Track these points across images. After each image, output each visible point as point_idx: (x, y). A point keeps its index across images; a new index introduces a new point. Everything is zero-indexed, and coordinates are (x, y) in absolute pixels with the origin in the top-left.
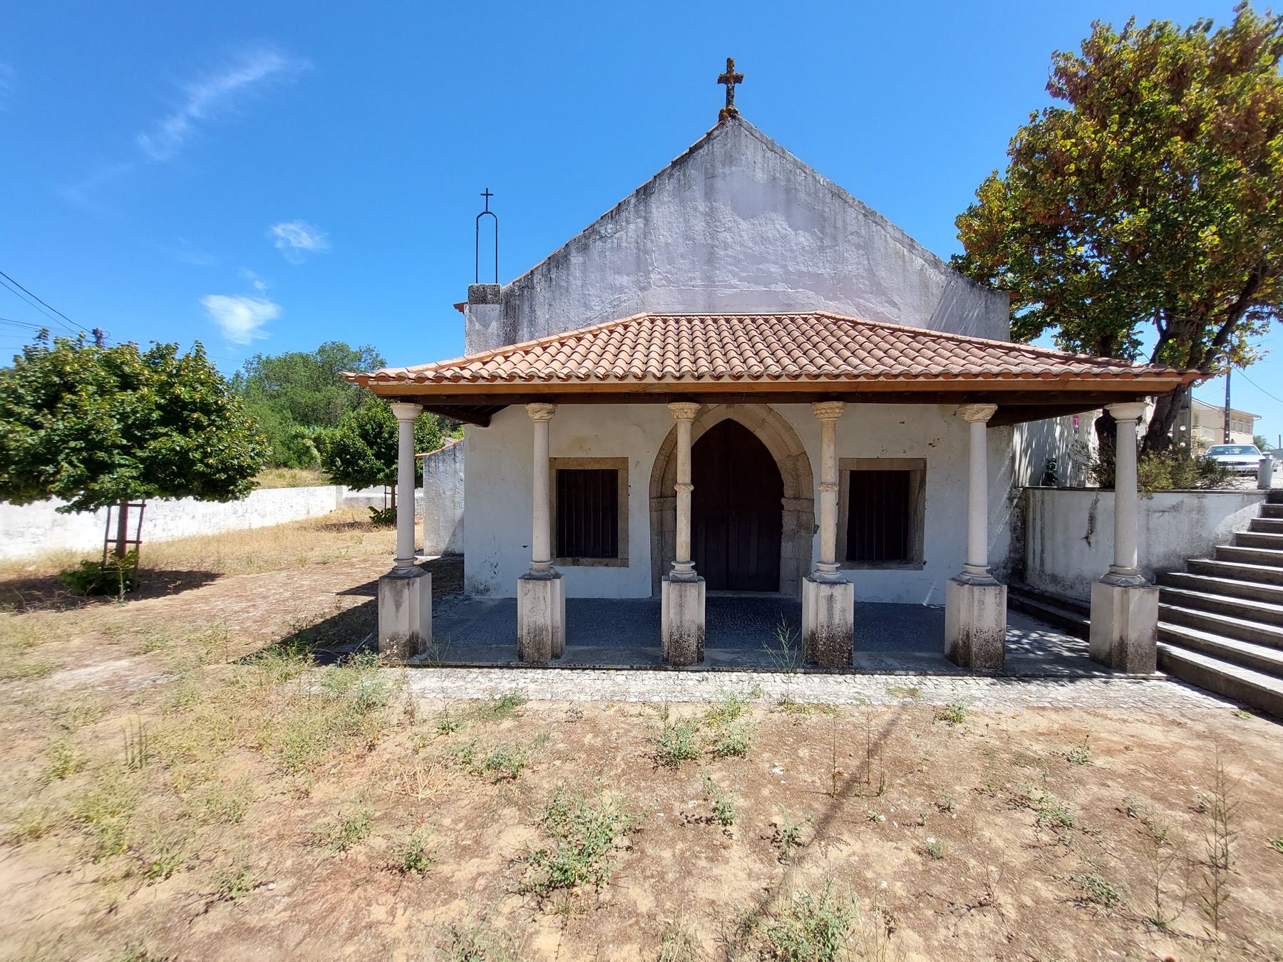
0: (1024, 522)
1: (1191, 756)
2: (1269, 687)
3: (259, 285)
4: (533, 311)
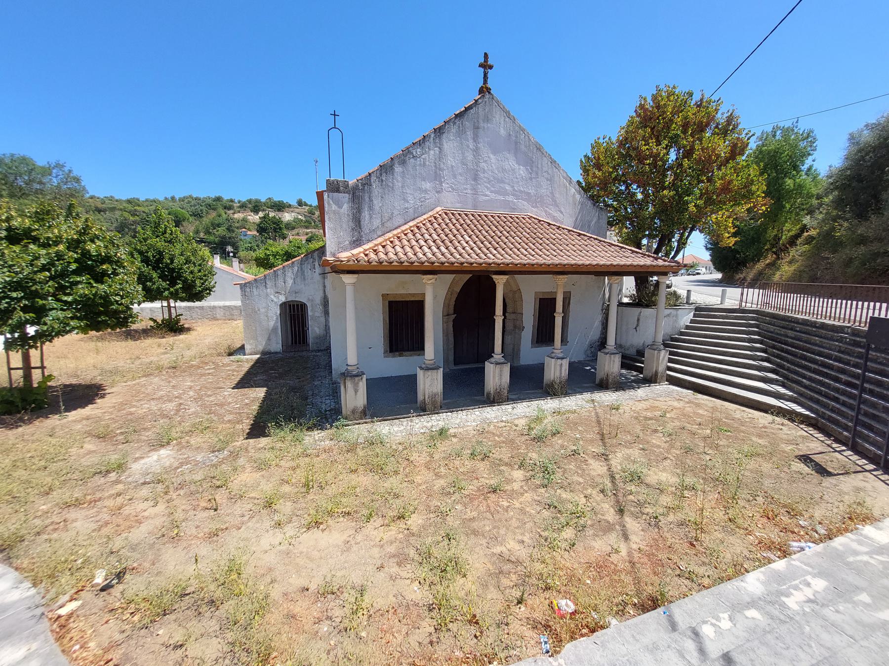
1: (689, 409)
4: (371, 200)
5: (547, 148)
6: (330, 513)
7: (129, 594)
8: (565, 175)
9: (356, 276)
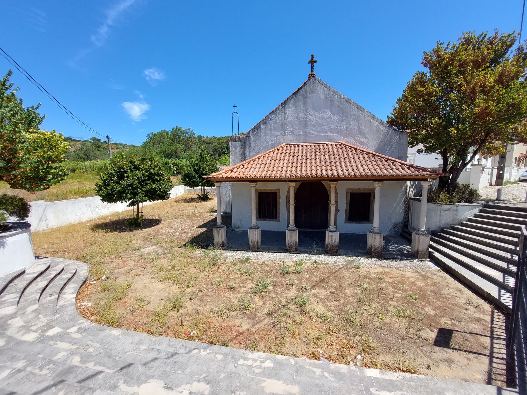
0: (409, 210)
2: (448, 264)
3: (141, 96)
4: (250, 144)
5: (354, 100)
8: (369, 114)
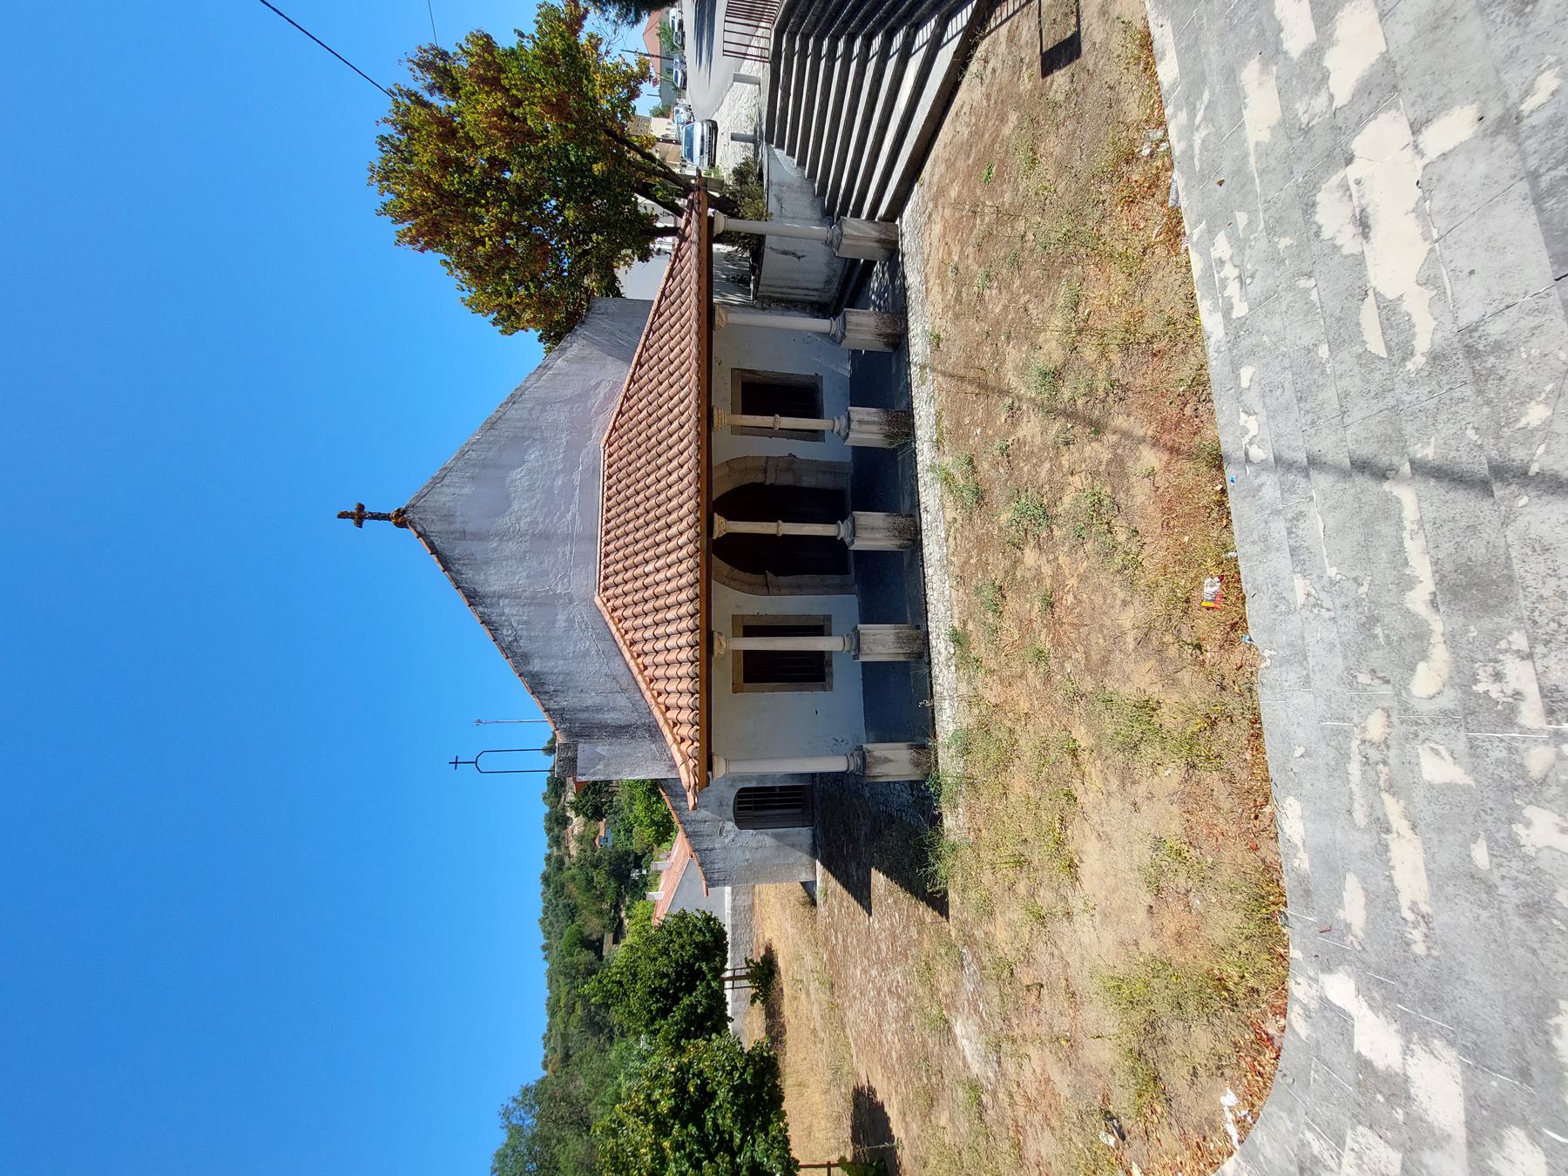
0: (779, 301)
4: (586, 709)
5: (490, 410)
6: (1060, 843)
7: (1132, 1112)
9: (715, 759)
